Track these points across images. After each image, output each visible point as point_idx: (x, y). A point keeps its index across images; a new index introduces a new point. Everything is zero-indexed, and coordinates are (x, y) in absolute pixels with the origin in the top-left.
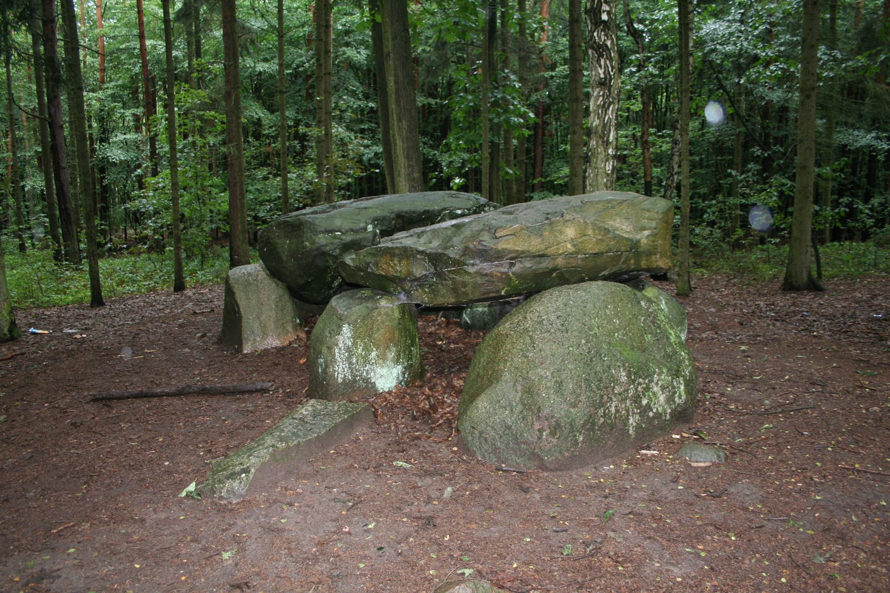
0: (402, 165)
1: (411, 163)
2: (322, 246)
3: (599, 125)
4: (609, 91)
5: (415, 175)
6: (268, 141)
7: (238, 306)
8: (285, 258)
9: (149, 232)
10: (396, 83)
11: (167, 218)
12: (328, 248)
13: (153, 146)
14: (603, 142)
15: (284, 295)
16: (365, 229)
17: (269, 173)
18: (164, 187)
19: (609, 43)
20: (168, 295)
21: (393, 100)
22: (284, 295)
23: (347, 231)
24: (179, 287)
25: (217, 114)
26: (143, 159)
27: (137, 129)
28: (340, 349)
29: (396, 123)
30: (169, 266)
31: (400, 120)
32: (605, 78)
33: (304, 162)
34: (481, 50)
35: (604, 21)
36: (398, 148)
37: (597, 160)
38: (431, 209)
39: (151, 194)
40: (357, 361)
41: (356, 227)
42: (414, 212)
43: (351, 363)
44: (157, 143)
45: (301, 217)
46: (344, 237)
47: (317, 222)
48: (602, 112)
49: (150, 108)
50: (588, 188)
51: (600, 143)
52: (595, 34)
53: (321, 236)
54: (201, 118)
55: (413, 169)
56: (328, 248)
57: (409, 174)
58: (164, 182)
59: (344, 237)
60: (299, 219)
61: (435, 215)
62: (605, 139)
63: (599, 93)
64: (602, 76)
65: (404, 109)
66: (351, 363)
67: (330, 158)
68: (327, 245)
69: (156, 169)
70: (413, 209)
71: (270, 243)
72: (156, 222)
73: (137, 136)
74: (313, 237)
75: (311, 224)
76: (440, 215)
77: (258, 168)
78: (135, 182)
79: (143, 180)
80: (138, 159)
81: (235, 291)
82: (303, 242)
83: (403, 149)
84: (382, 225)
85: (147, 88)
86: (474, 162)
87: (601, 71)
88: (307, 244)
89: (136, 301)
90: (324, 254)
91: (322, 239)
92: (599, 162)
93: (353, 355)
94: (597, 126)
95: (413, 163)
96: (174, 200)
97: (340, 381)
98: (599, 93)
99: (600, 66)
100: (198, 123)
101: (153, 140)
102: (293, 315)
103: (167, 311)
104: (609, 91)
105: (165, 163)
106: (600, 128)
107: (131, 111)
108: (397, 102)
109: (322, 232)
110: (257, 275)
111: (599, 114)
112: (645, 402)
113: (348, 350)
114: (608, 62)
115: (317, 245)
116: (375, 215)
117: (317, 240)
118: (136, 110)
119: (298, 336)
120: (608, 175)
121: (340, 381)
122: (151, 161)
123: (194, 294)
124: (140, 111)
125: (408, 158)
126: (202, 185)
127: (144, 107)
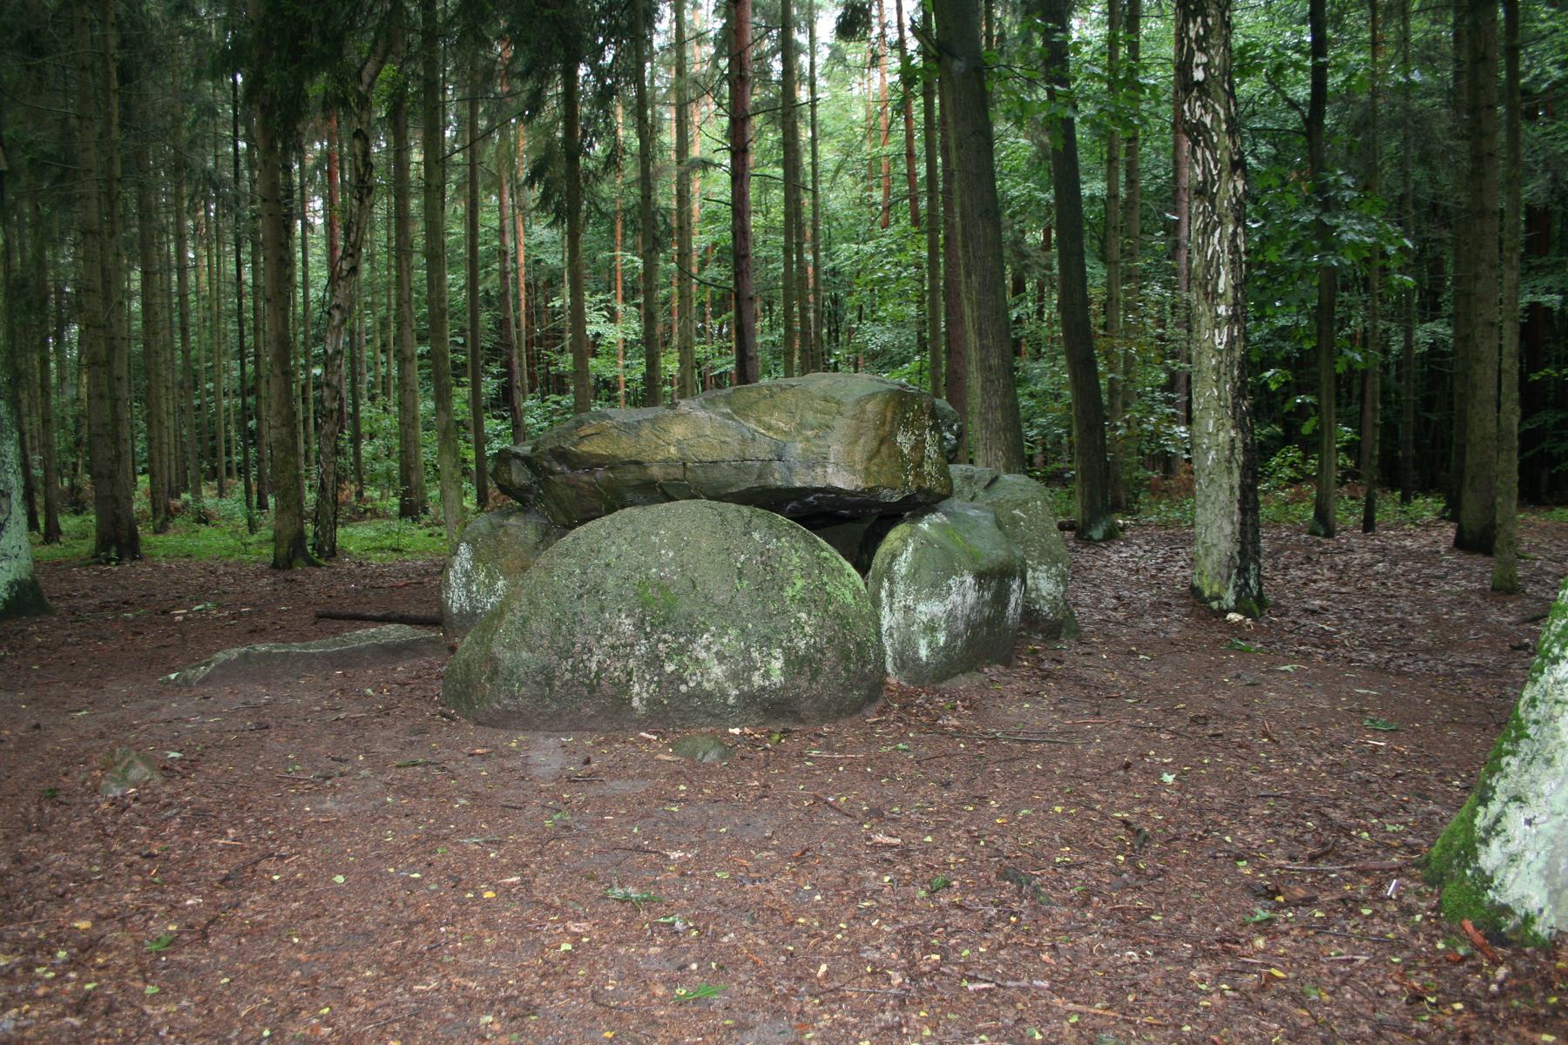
1: (985, 342)
4: (1212, 202)
10: (962, 216)
14: (1207, 294)
19: (1208, 120)
21: (959, 244)
28: (456, 572)
31: (968, 275)
32: (1205, 182)
34: (752, 172)
35: (1198, 83)
37: (1199, 326)
40: (478, 590)
43: (469, 591)
51: (1202, 296)
52: (1186, 107)
62: (1210, 289)
63: (1198, 208)
64: (1200, 178)
66: (469, 591)
87: (1198, 171)
92: (1202, 330)
95: (989, 342)
97: (455, 611)
98: (1198, 208)
99: (1197, 161)
104: (1212, 202)
112: (670, 668)
113: (466, 573)
114: (1208, 153)
121: (455, 611)
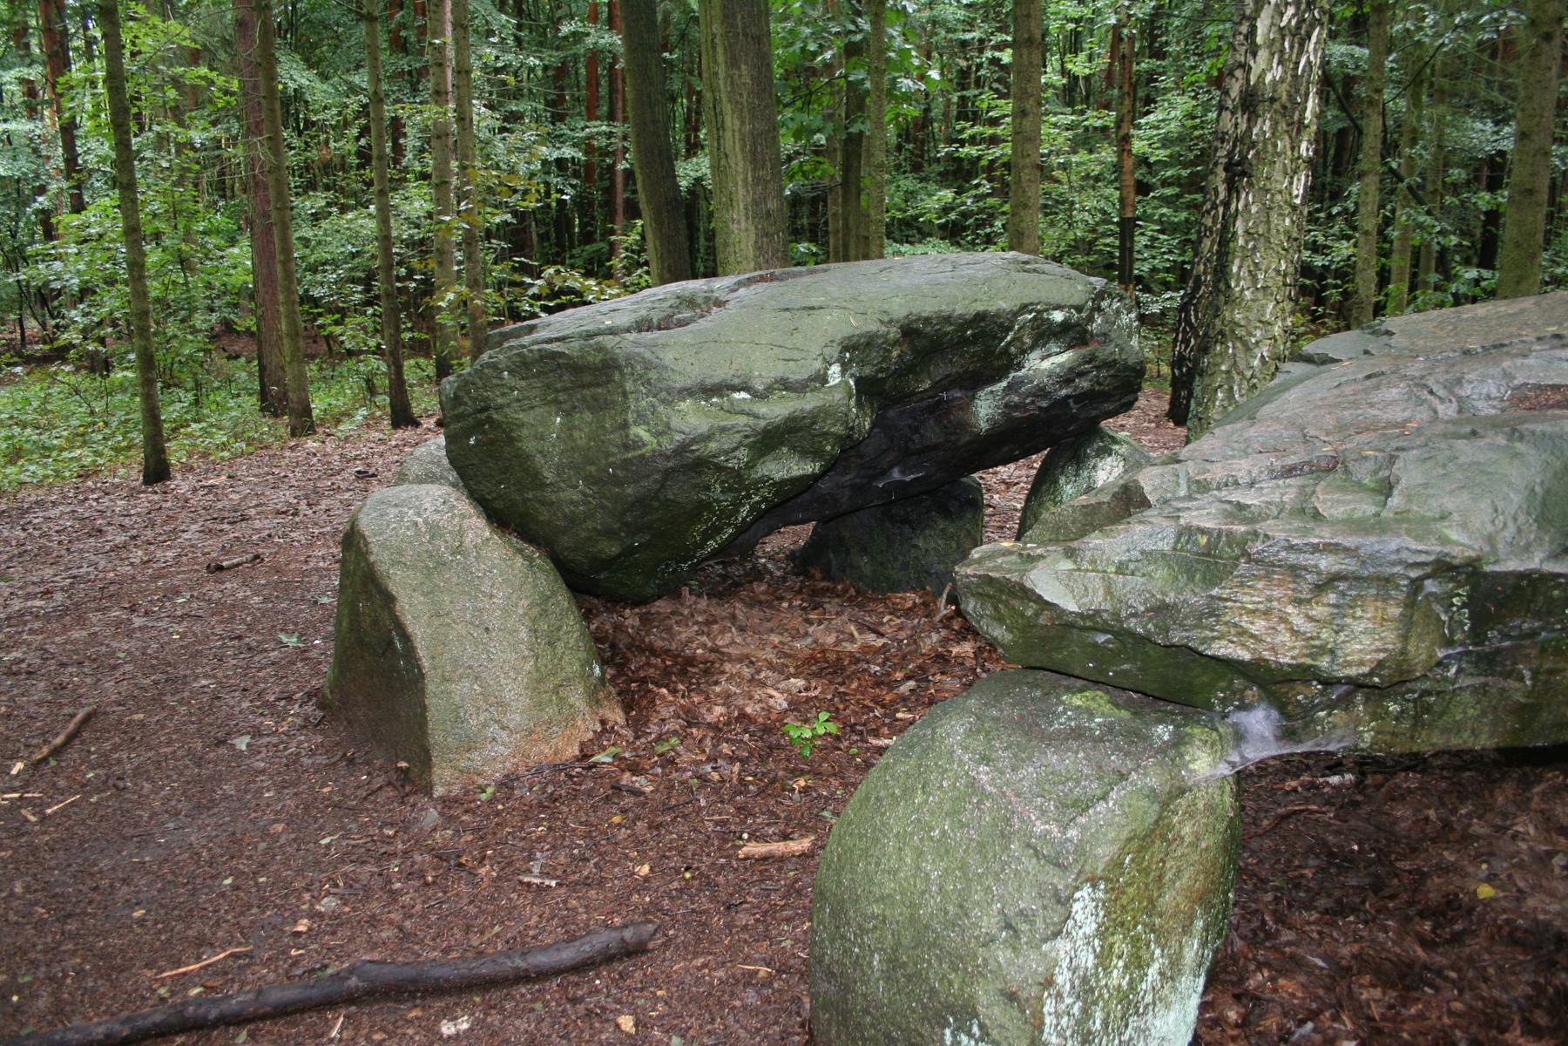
0: (740, 178)
2: (694, 441)
3: (1282, 80)
5: (770, 205)
6: (323, 137)
7: (406, 638)
8: (549, 476)
9: (73, 336)
11: (112, 302)
12: (713, 446)
13: (69, 146)
15: (554, 593)
16: (822, 379)
17: (329, 205)
18: (101, 236)
20: (133, 494)
22: (554, 593)
23: (770, 389)
24: (157, 472)
25: (215, 73)
26: (50, 177)
27: (32, 112)
29: (722, 70)
30: (129, 406)
33: (405, 180)
36: (728, 134)
38: (992, 309)
39: (73, 250)
41: (797, 373)
42: (947, 319)
44: (78, 143)
45: (609, 341)
46: (762, 409)
47: (668, 357)
48: (1292, 47)
49: (58, 61)
50: (1241, 242)
51: (1283, 126)
53: (686, 405)
54: (176, 82)
55: (765, 189)
56: (713, 446)
57: (755, 203)
58: (100, 224)
59: (762, 409)
60: (600, 349)
61: (1001, 326)
65: (745, 35)
67: (470, 170)
68: (707, 438)
69: (80, 196)
70: (946, 309)
71: (489, 420)
72: (88, 314)
73: (31, 126)
74: (661, 408)
75: (648, 366)
76: (1010, 329)
77: (305, 192)
78: (35, 224)
79: (54, 220)
80: (37, 177)
81: (393, 588)
82: (625, 426)
83: (743, 139)
84: (862, 363)
85: (47, 20)
86: (799, 177)
88: (640, 432)
89: (53, 513)
90: (701, 465)
91: (691, 418)
92: (1278, 176)
93: (1095, 1003)
94: (1274, 83)
96: (136, 266)
100: (172, 93)
101: (68, 131)
102: (582, 655)
103: (138, 555)
105: (98, 185)
106: (1283, 90)
107: (14, 73)
108: (725, 16)
109: (687, 392)
110: (461, 533)
111: (1282, 51)
115: (679, 437)
116: (847, 332)
117: (675, 422)
118: (26, 70)
119: (603, 722)
120: (1294, 208)
122: (68, 177)
123: (195, 490)
124: (35, 73)
125: (754, 161)
126: (188, 232)
127: (44, 64)
